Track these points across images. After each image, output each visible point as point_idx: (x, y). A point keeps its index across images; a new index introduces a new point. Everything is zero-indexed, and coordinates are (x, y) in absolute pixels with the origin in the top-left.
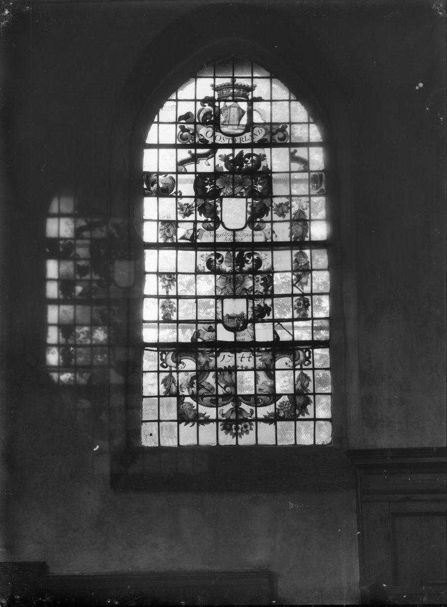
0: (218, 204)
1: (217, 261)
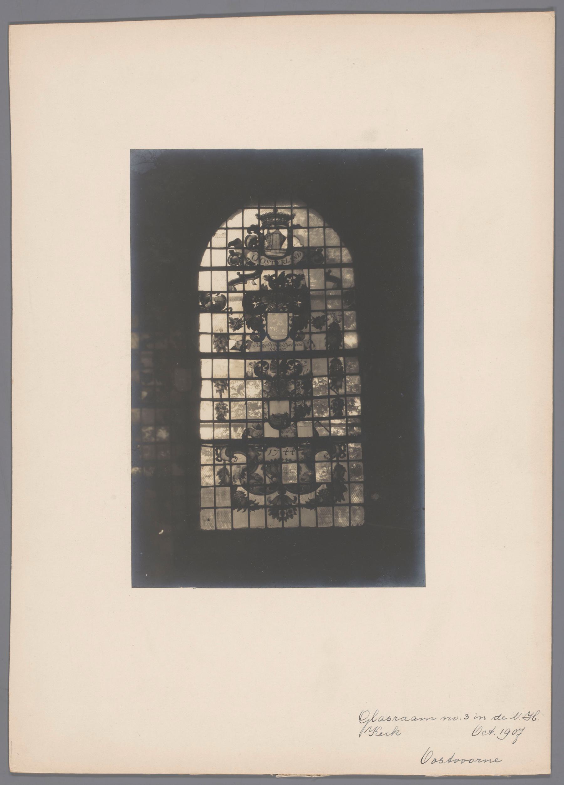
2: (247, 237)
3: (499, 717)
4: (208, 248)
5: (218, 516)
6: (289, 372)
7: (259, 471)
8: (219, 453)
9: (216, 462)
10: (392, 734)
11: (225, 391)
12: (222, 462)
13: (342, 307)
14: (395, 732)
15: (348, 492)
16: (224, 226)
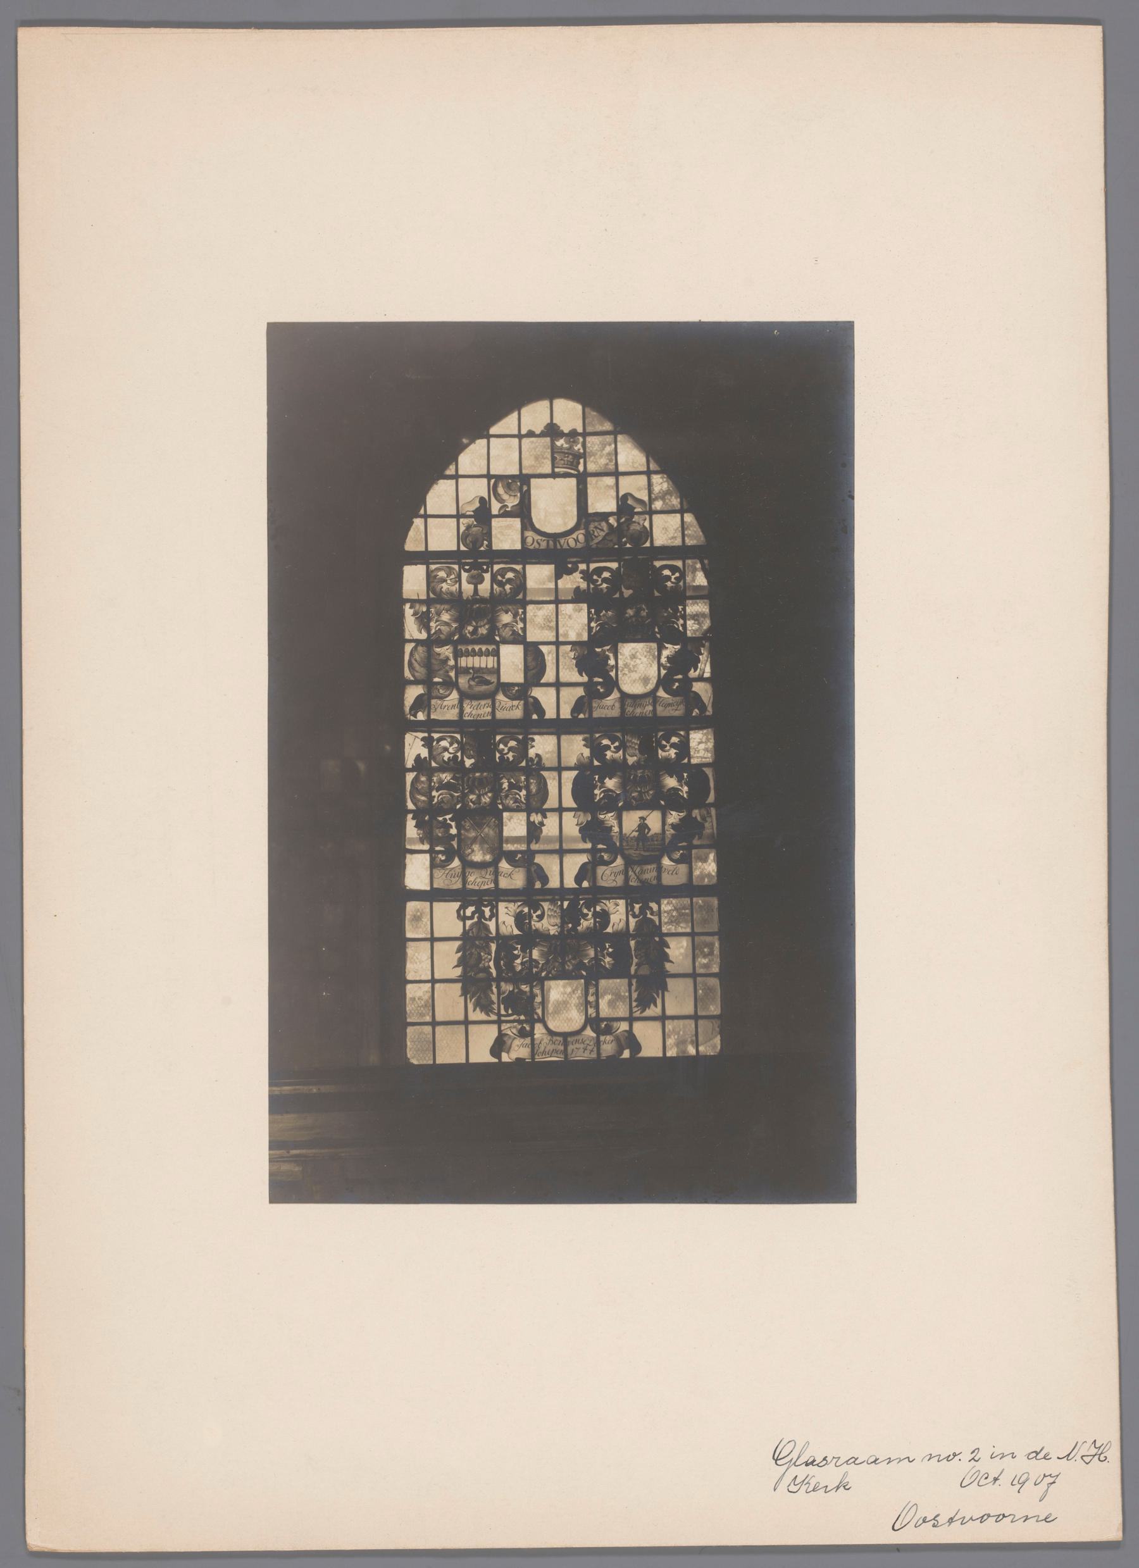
0: (537, 991)
3: (1037, 1454)
4: (421, 516)
5: (450, 1030)
6: (585, 924)
10: (838, 1488)
13: (696, 1011)
14: (843, 1486)
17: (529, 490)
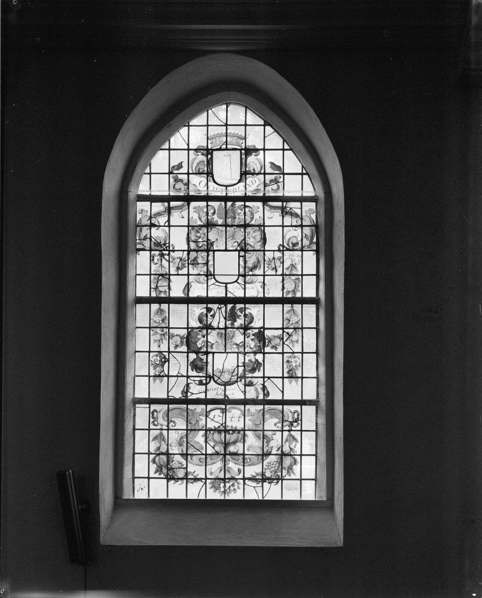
1: (209, 315)
2: (194, 159)
7: (199, 438)
8: (155, 416)
9: (152, 427)
11: (164, 341)
12: (159, 427)
15: (299, 465)
16: (148, 171)
17: (212, 157)
